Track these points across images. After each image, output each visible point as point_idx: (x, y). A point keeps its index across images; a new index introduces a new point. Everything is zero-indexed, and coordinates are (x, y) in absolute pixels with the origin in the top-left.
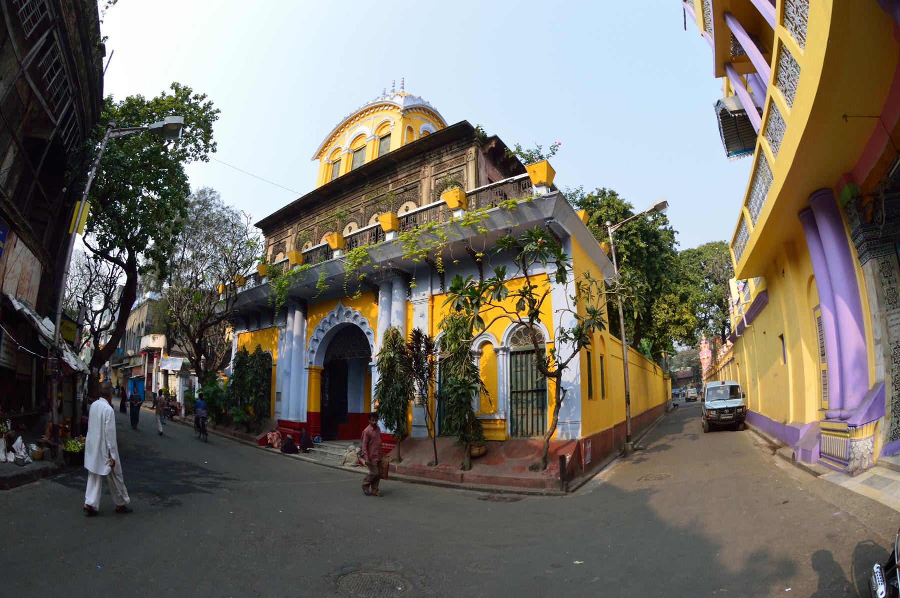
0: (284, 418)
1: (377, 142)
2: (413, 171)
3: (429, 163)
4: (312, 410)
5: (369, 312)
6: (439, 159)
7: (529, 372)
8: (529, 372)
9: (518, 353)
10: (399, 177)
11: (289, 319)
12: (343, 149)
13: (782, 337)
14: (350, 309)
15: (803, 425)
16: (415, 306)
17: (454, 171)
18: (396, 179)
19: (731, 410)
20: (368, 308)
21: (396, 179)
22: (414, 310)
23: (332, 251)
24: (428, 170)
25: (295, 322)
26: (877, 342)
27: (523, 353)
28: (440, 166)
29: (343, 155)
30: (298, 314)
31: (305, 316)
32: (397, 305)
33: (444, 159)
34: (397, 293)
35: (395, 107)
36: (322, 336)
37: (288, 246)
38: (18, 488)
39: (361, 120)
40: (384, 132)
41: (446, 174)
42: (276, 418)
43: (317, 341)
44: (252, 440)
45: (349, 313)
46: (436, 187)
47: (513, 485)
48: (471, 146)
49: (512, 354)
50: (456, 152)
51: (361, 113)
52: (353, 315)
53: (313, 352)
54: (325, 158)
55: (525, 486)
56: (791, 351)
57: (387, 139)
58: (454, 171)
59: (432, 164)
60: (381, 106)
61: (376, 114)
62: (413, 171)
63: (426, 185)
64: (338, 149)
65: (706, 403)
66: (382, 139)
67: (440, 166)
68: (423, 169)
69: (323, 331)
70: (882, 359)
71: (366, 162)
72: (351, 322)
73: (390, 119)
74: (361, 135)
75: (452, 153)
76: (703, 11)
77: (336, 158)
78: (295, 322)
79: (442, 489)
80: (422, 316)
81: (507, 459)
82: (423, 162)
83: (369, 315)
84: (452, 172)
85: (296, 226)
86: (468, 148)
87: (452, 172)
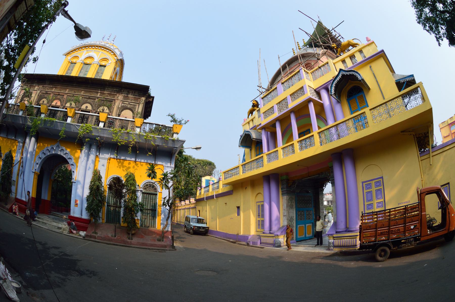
0: (19, 197)
1: (98, 66)
2: (113, 93)
3: (122, 94)
4: (33, 196)
5: (74, 154)
6: (127, 94)
7: (149, 202)
8: (149, 202)
9: (145, 193)
10: (105, 92)
11: (27, 140)
12: (80, 59)
13: (238, 208)
14: (64, 148)
15: (250, 235)
16: (100, 160)
17: (132, 104)
18: (103, 92)
19: (204, 228)
20: (74, 151)
21: (103, 92)
22: (99, 161)
23: (41, 113)
24: (120, 97)
25: (31, 144)
26: (284, 216)
27: (148, 193)
28: (126, 98)
29: (79, 61)
30: (33, 139)
31: (37, 141)
32: (92, 157)
33: (129, 96)
34: (93, 150)
35: (114, 54)
36: (44, 156)
37: (33, 95)
38: (85, 205)
39: (95, 49)
40: (103, 63)
41: (128, 103)
42: (13, 196)
43: (41, 158)
44: (4, 207)
45: (62, 150)
46: (122, 107)
47: (154, 247)
48: (144, 97)
49: (143, 193)
50: (136, 95)
51: (97, 46)
52: (65, 152)
53: (37, 164)
54: (69, 57)
55: (158, 247)
56: (243, 212)
57: (103, 67)
58: (132, 104)
59: (123, 95)
60: (108, 49)
61: (103, 51)
62: (113, 93)
63: (118, 104)
64: (76, 57)
65: (191, 223)
66: (101, 66)
67: (126, 98)
68: (118, 95)
69: (45, 154)
70: (286, 220)
71: (71, 75)
72: (62, 155)
73: (109, 59)
74: (90, 57)
75: (134, 95)
76: (297, 91)
77: (74, 61)
78: (31, 144)
79: (116, 246)
80: (103, 165)
81: (145, 236)
82: (120, 92)
83: (74, 156)
84: (131, 103)
85: (41, 86)
86: (142, 97)
87: (131, 103)
